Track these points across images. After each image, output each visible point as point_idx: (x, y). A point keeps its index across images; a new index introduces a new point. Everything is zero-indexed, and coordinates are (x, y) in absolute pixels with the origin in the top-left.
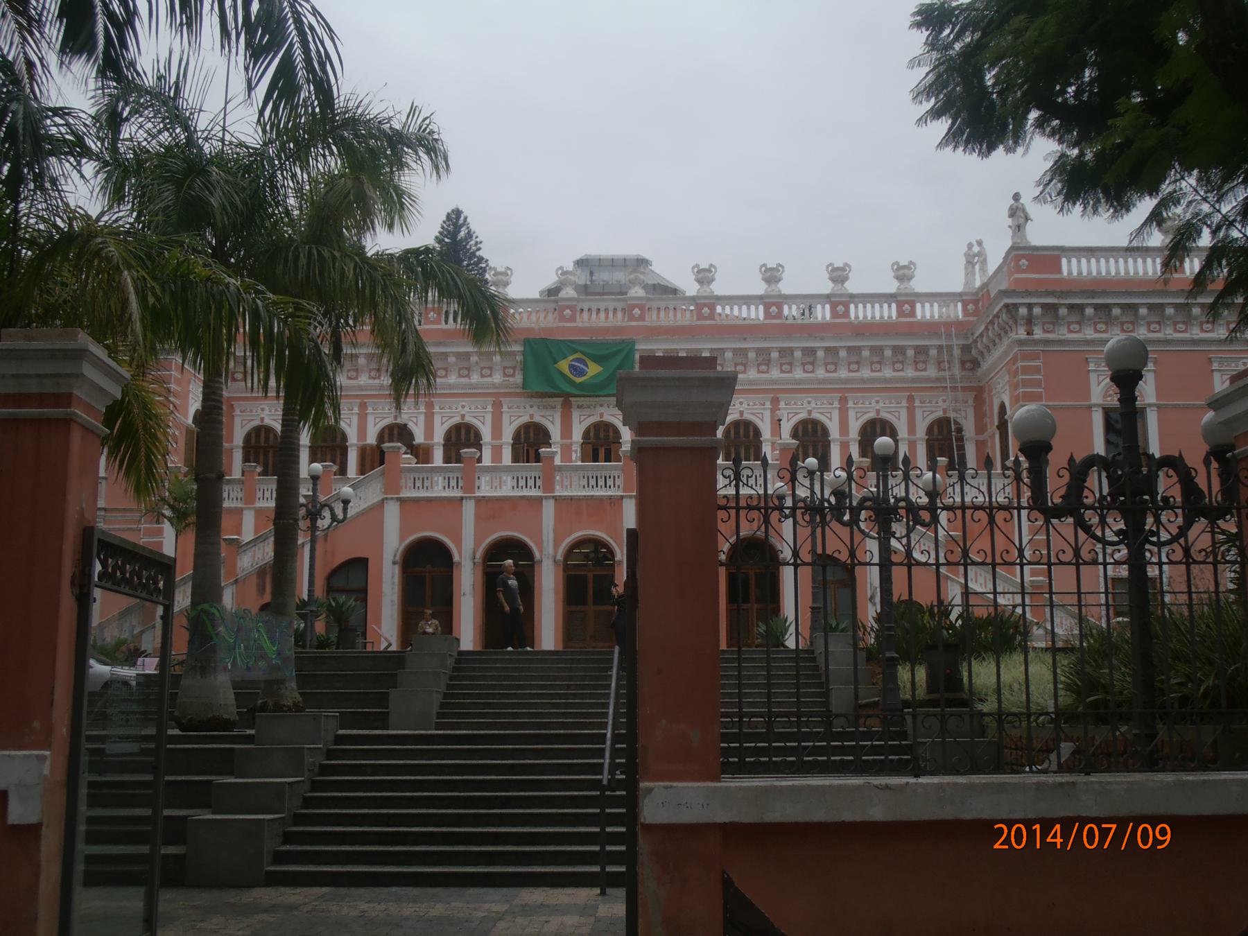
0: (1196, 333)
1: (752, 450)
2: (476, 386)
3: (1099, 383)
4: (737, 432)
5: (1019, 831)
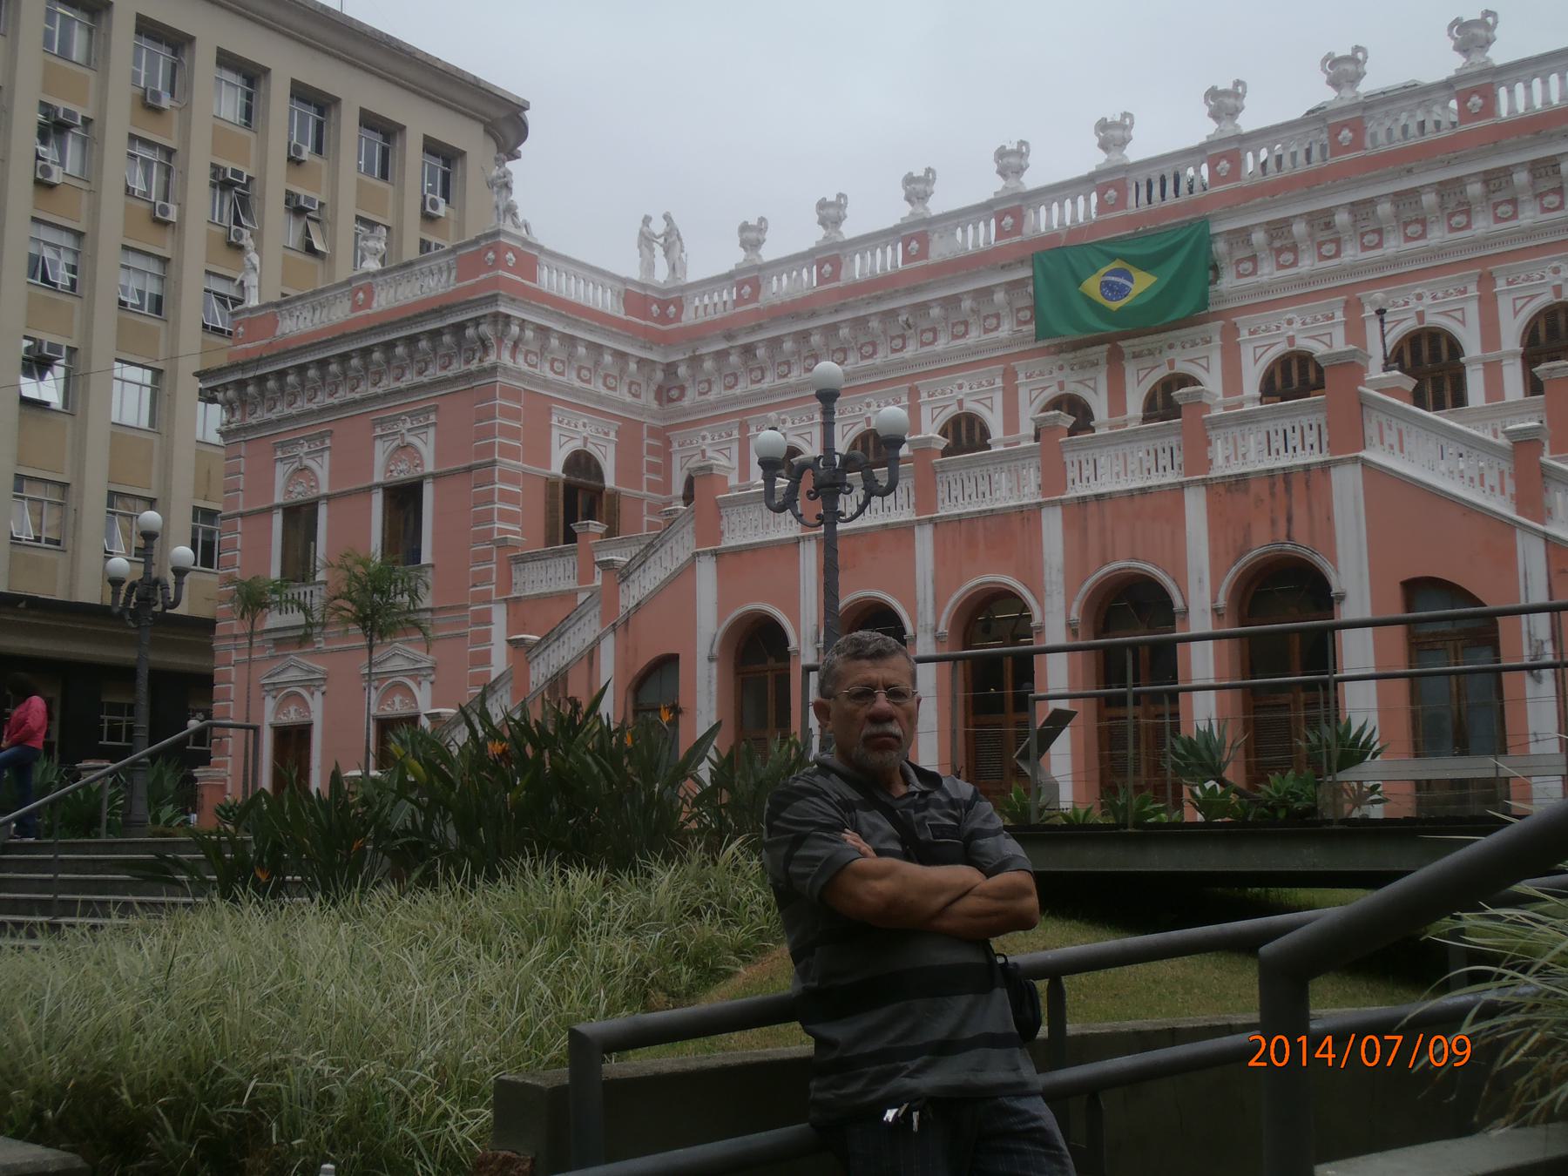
1: (1448, 386)
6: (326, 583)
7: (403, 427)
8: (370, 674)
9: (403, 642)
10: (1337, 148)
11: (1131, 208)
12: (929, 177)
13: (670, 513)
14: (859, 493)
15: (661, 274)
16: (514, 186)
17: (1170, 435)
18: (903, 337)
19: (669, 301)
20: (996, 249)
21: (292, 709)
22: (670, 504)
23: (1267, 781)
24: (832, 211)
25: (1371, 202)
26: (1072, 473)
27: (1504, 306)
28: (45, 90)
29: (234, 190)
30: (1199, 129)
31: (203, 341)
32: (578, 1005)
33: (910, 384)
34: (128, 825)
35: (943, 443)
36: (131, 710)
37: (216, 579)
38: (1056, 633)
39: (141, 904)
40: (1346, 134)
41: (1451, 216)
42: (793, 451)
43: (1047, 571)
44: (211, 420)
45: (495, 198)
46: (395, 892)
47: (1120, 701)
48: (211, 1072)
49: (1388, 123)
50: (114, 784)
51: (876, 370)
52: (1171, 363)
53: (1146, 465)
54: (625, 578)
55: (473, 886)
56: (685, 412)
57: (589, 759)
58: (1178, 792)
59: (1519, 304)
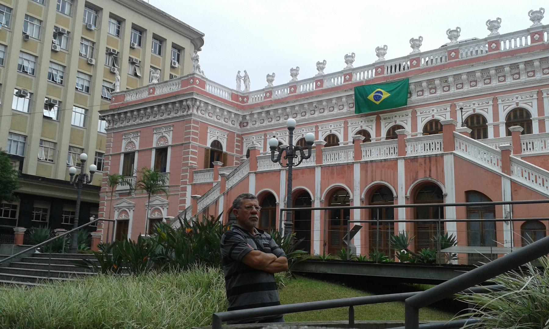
1: (482, 132)
2: (481, 91)
4: (515, 116)
6: (136, 177)
7: (162, 131)
8: (148, 205)
9: (160, 196)
10: (450, 58)
11: (385, 74)
12: (297, 69)
13: (242, 160)
14: (299, 156)
15: (243, 88)
16: (199, 60)
17: (394, 144)
18: (314, 110)
19: (245, 97)
20: (344, 85)
21: (123, 215)
22: (242, 157)
23: (421, 250)
24: (294, 72)
26: (364, 154)
27: (501, 108)
28: (56, 22)
29: (113, 56)
30: (408, 51)
31: (101, 101)
32: (210, 309)
33: (316, 125)
34: (71, 249)
35: (325, 143)
36: (73, 213)
37: (102, 174)
38: (357, 202)
39: (78, 274)
40: (453, 54)
41: (485, 80)
42: (280, 143)
43: (355, 183)
44: (103, 125)
45: (194, 63)
46: (156, 273)
47: (375, 223)
48: (101, 325)
49: (466, 50)
50: (68, 236)
51: (306, 120)
52: (396, 122)
53: (386, 152)
54: (228, 179)
55: (180, 271)
56: (248, 130)
57: (216, 234)
58: (393, 252)
59: (505, 107)
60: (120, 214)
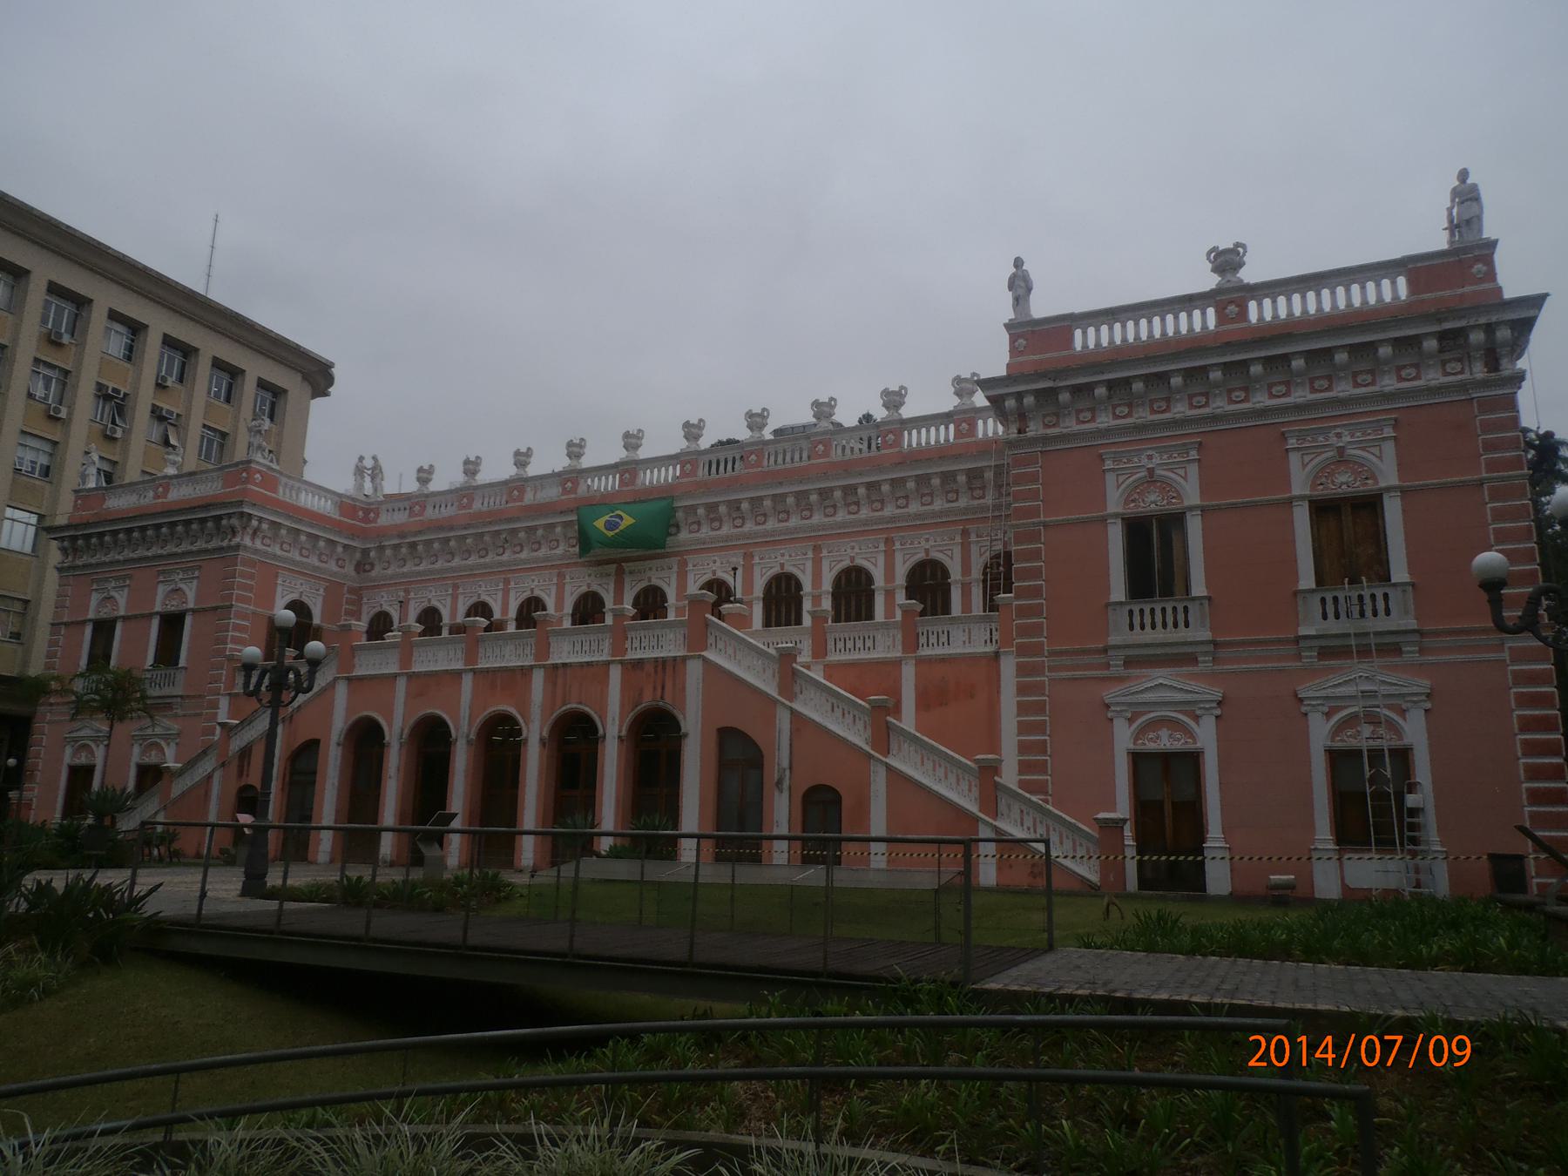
0: (1433, 377)
3: (1304, 466)
4: (778, 587)
5: (1280, 1044)
12: (529, 453)
25: (761, 498)
27: (825, 565)
29: (115, 403)
33: (817, 542)
40: (821, 447)
60: (75, 753)
